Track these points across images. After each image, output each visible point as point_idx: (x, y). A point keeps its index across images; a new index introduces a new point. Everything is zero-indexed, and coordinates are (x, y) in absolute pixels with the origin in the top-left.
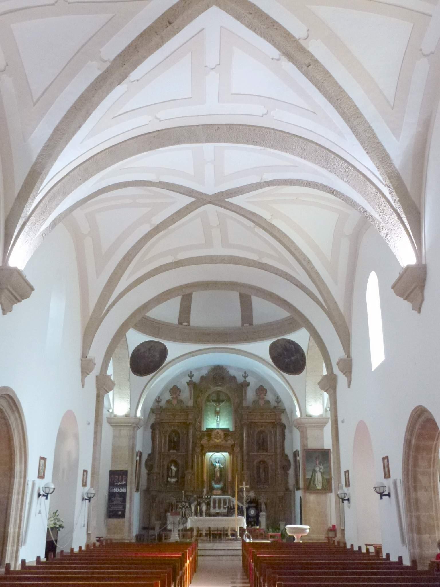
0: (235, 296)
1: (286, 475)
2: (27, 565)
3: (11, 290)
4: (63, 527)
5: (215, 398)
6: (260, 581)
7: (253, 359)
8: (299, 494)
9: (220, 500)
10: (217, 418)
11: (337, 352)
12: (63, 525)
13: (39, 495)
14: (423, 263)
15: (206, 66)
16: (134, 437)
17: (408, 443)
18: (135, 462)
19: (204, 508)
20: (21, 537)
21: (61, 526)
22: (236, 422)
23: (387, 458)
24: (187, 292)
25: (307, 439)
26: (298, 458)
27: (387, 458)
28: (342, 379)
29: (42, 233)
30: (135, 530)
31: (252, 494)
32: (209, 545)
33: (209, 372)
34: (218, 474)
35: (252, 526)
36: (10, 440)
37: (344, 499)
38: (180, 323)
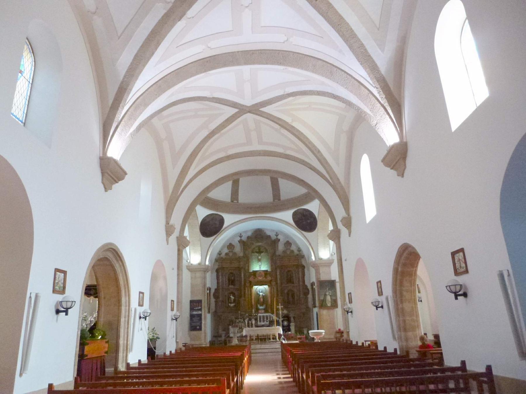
0: (267, 179)
1: (306, 299)
2: (131, 366)
3: (110, 173)
4: (159, 338)
5: (257, 251)
6: (298, 371)
7: (281, 224)
8: (316, 310)
9: (263, 317)
10: (260, 263)
11: (339, 213)
12: (159, 336)
13: (140, 318)
14: (405, 140)
15: (242, 5)
16: (205, 278)
17: (396, 271)
18: (206, 294)
19: (254, 322)
20: (129, 347)
21: (158, 338)
22: (272, 266)
23: (380, 282)
24: (235, 177)
25: (320, 274)
26: (314, 287)
27: (380, 282)
28: (344, 231)
29: (131, 134)
30: (209, 338)
31: (285, 312)
32: (258, 346)
33: (252, 234)
34: (262, 300)
35: (286, 332)
36: (117, 280)
37: (348, 312)
38: (232, 201)
